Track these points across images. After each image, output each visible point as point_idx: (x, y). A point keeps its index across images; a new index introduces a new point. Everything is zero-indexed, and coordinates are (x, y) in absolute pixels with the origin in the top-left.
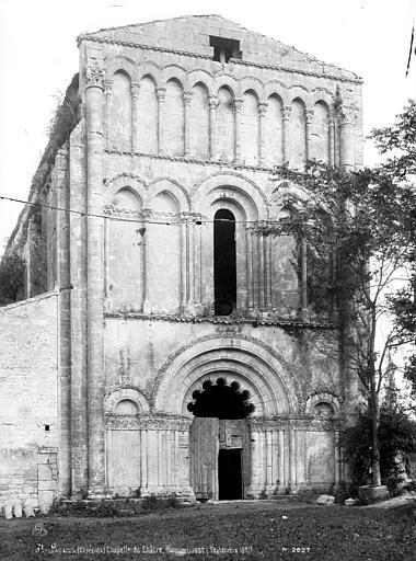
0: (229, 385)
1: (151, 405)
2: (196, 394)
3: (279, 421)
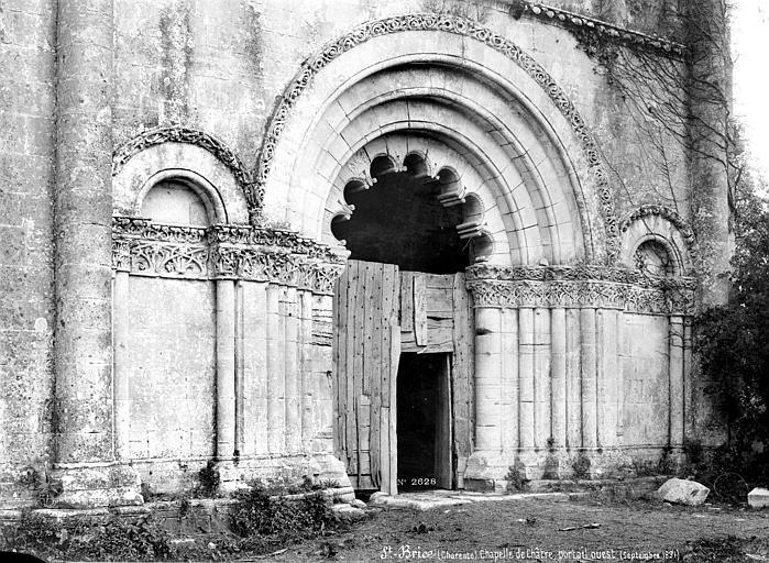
0: (433, 173)
1: (253, 203)
2: (352, 191)
3: (558, 280)
